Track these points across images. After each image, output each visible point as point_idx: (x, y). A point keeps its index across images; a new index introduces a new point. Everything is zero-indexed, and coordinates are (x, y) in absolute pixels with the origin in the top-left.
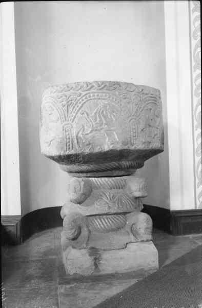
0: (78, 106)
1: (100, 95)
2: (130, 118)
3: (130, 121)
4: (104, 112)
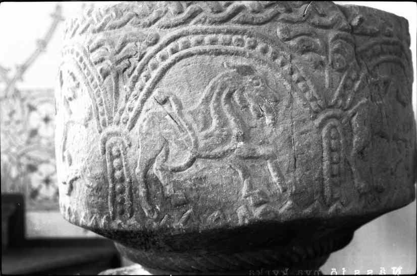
0: (147, 78)
1: (221, 37)
2: (321, 117)
3: (321, 126)
4: (236, 96)
